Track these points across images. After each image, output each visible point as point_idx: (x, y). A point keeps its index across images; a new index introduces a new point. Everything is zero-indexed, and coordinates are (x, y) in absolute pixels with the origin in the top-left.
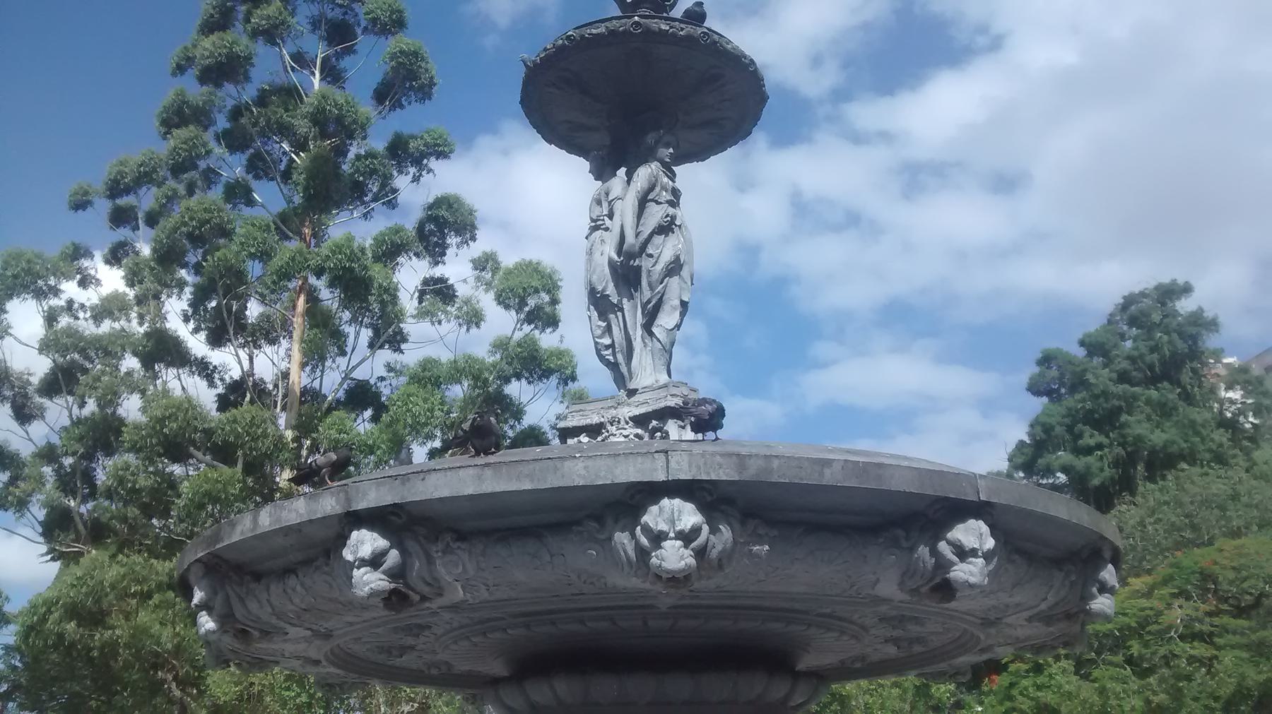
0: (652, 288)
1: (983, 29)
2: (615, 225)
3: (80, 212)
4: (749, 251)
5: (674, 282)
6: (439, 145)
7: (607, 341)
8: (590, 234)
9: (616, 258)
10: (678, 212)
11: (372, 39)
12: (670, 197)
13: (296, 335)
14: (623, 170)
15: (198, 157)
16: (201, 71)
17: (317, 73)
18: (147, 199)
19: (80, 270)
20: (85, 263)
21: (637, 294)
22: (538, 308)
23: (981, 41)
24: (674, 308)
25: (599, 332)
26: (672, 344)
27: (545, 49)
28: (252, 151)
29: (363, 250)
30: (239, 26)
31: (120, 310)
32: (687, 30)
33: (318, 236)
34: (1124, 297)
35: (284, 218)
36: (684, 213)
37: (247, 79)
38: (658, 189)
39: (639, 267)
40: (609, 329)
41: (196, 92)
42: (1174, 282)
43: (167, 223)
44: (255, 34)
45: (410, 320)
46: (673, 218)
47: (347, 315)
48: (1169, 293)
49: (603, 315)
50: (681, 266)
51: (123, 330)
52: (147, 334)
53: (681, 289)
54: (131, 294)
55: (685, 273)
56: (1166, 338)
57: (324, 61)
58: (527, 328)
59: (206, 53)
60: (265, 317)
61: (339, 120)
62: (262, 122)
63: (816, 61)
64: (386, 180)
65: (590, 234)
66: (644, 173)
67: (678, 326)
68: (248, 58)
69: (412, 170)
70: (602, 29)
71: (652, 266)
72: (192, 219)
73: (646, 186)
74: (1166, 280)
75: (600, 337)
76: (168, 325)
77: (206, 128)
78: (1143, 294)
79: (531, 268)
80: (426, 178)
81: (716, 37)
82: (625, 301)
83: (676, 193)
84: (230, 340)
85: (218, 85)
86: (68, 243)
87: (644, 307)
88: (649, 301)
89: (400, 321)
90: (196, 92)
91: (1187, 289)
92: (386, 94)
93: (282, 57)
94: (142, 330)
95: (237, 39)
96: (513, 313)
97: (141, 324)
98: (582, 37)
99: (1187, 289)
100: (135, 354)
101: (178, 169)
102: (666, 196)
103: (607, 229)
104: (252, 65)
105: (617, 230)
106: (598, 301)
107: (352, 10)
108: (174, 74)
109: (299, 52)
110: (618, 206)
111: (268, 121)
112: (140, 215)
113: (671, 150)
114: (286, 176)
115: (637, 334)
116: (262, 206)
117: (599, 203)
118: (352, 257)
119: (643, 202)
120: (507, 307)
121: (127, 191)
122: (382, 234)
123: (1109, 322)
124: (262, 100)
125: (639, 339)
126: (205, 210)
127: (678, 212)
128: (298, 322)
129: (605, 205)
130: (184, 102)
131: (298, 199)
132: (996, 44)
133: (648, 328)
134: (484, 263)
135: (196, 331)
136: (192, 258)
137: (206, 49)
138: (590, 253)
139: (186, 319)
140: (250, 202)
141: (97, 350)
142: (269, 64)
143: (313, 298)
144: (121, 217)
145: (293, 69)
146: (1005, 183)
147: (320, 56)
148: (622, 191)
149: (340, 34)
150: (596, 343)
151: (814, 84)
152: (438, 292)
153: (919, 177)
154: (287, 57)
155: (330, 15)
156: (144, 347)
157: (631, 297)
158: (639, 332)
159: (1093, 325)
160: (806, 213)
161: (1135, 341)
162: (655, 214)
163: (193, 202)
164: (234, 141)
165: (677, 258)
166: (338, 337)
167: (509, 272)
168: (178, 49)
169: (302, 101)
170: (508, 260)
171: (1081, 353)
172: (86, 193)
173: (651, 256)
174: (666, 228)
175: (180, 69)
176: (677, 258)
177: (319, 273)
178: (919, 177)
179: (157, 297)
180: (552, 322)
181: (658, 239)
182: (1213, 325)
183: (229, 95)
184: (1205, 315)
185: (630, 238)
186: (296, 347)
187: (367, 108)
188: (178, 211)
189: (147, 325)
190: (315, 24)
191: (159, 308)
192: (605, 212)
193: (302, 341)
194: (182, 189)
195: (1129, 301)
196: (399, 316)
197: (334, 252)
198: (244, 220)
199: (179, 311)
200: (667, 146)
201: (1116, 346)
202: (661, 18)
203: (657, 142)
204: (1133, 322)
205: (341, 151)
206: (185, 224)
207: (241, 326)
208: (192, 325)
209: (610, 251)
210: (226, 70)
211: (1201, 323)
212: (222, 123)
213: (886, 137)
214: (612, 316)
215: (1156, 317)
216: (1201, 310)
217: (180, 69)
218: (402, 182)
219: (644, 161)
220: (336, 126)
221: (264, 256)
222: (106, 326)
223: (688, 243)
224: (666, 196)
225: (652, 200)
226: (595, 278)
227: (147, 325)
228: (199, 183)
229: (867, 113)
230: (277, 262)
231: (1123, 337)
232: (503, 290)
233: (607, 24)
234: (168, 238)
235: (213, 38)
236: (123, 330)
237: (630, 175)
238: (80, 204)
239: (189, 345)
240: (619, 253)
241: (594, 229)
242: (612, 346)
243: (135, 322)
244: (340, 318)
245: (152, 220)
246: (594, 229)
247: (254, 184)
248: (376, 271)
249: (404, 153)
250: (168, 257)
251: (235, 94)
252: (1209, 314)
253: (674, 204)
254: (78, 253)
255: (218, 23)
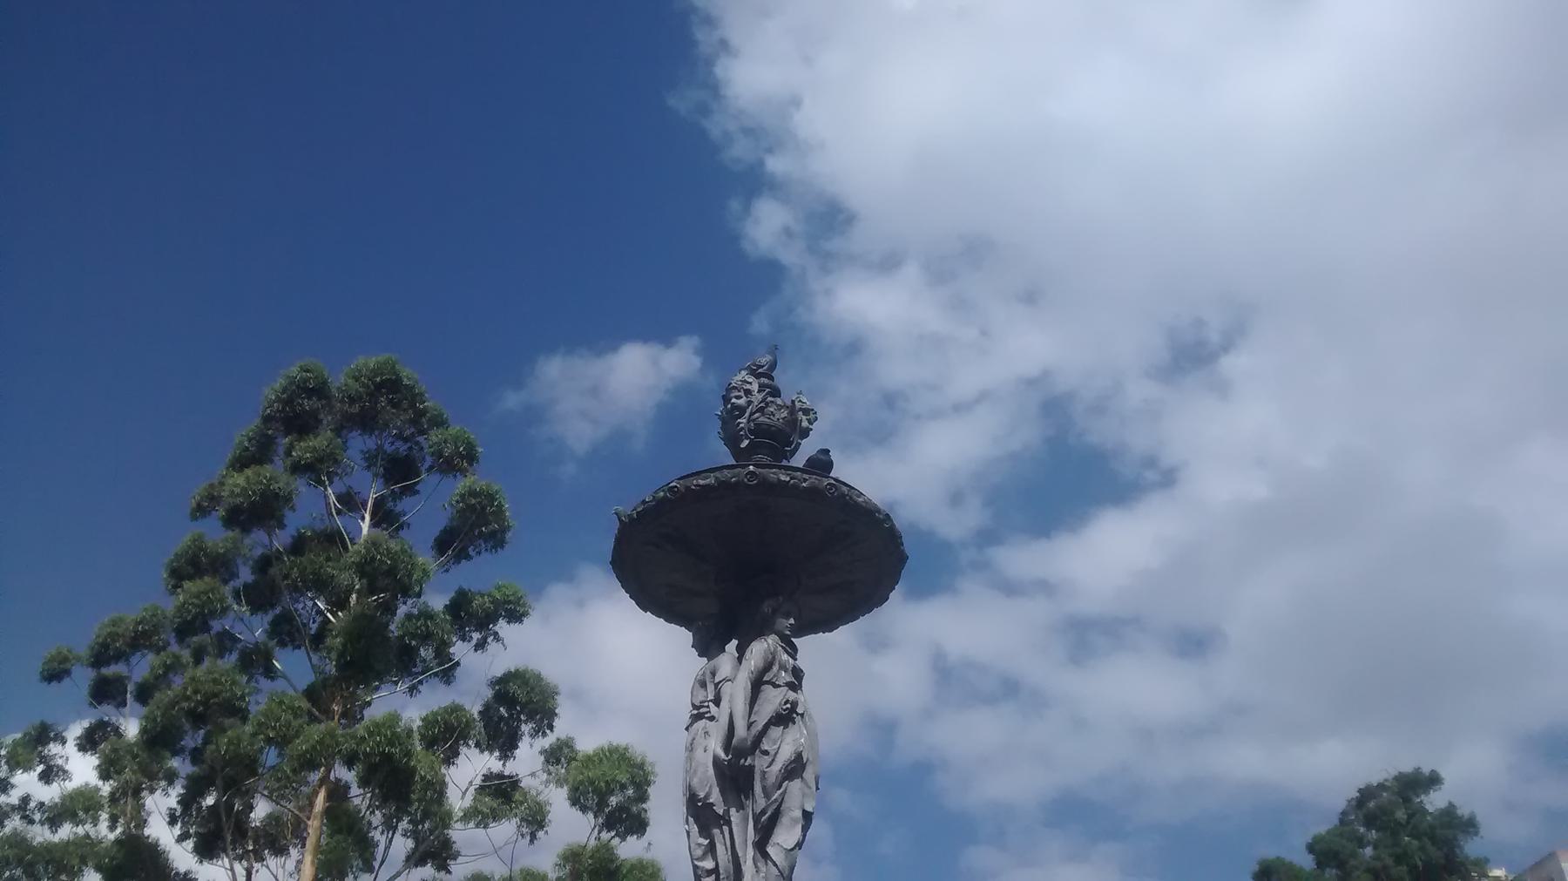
0: (767, 795)
1: (1151, 462)
2: (722, 713)
3: (54, 684)
4: (884, 729)
5: (795, 786)
6: (510, 602)
7: (709, 864)
8: (691, 725)
9: (723, 755)
10: (800, 697)
11: (434, 478)
12: (790, 678)
13: (310, 843)
14: (735, 642)
15: (213, 614)
16: (227, 511)
17: (367, 517)
18: (142, 667)
19: (44, 759)
20: (54, 748)
21: (749, 803)
22: (621, 808)
23: (1151, 475)
24: (795, 821)
25: (699, 852)
26: (792, 869)
27: (644, 502)
28: (278, 610)
29: (410, 732)
30: (278, 461)
31: (87, 811)
32: (809, 481)
33: (351, 716)
34: (1360, 790)
35: (311, 693)
36: (808, 697)
37: (282, 526)
38: (775, 668)
39: (752, 767)
40: (711, 849)
41: (216, 535)
42: (1417, 771)
43: (163, 697)
44: (297, 469)
45: (458, 825)
46: (795, 704)
47: (377, 818)
48: (1416, 783)
49: (705, 831)
50: (803, 767)
51: (87, 836)
52: (118, 842)
53: (804, 795)
54: (106, 788)
55: (809, 774)
56: (1415, 842)
57: (378, 503)
58: (605, 836)
59: (237, 490)
60: (272, 819)
61: (391, 572)
62: (295, 573)
63: (956, 499)
64: (442, 653)
65: (691, 725)
66: (758, 650)
67: (799, 845)
68: (288, 499)
69: (476, 636)
70: (711, 480)
71: (769, 767)
72: (196, 692)
73: (761, 664)
74: (1407, 767)
75: (701, 859)
76: (147, 832)
77: (226, 582)
78: (1381, 787)
79: (618, 756)
80: (492, 646)
81: (845, 489)
82: (733, 811)
83: (797, 673)
84: (225, 851)
85: (246, 530)
86: (37, 722)
87: (757, 819)
88: (763, 812)
89: (447, 826)
90: (216, 535)
91: (1434, 780)
92: (453, 544)
93: (326, 497)
94: (112, 837)
95: (275, 473)
96: (591, 815)
97: (112, 828)
98: (688, 488)
99: (1434, 780)
100: (98, 869)
101: (184, 631)
102: (785, 677)
103: (712, 718)
104: (293, 509)
105: (724, 720)
106: (701, 814)
107: (417, 443)
108: (194, 518)
109: (348, 494)
110: (726, 689)
111: (302, 572)
112: (129, 688)
113: (792, 621)
114: (318, 640)
115: (748, 855)
116: (285, 677)
117: (703, 685)
118: (394, 740)
119: (757, 685)
120: (584, 809)
121: (120, 656)
122: (435, 714)
123: (1342, 822)
124: (298, 546)
125: (750, 862)
126: (215, 681)
127: (800, 697)
128: (314, 825)
129: (711, 687)
130: (201, 549)
131: (331, 668)
132: (1169, 479)
133: (761, 846)
134: (557, 755)
135: (181, 839)
136: (191, 740)
137: (237, 485)
138: (691, 748)
139: (172, 821)
140: (270, 672)
141: (48, 863)
142: (311, 505)
143: (338, 793)
144: (106, 692)
145: (339, 512)
146: (1194, 644)
147: (373, 496)
148: (735, 668)
149: (400, 472)
150: (695, 867)
151: (955, 525)
152: (500, 793)
153: (1088, 636)
154: (333, 498)
155: (388, 448)
156: (112, 859)
157: (741, 807)
158: (750, 852)
159: (1322, 827)
160: (953, 681)
161: (1375, 848)
162: (773, 699)
163: (200, 672)
164: (259, 597)
165: (799, 756)
166: (365, 848)
167: (589, 760)
168: (205, 485)
169: (346, 549)
170: (587, 744)
171: (1307, 862)
172: (66, 660)
173: (766, 753)
174: (785, 717)
175: (200, 511)
176: (799, 756)
177: (350, 762)
178: (1088, 636)
179: (137, 793)
180: (637, 825)
181: (775, 732)
182: (1470, 826)
183: (257, 542)
184: (1459, 812)
185: (741, 731)
186: (308, 859)
187: (425, 558)
188: (178, 682)
189: (119, 830)
190: (370, 459)
191: (140, 807)
192: (711, 697)
193: (318, 849)
194: (186, 655)
195: (1366, 794)
196: (445, 820)
197: (371, 734)
198: (260, 698)
199: (164, 811)
200: (787, 618)
201: (1354, 855)
202: (780, 467)
203: (775, 611)
204: (1370, 821)
205: (389, 609)
206: (188, 699)
207: (241, 829)
208: (177, 830)
209: (715, 745)
210: (260, 511)
211: (1456, 824)
212: (246, 575)
213: (1044, 587)
214: (716, 831)
215: (1401, 815)
216: (1451, 805)
217: (200, 511)
218: (460, 650)
219: (760, 633)
220: (388, 578)
221: (282, 742)
222: (66, 831)
223: (812, 736)
224: (785, 677)
225: (768, 682)
226: (695, 782)
227: (119, 830)
228: (210, 649)
229: (1021, 559)
230: (301, 745)
231: (1361, 843)
232: (581, 782)
233: (718, 474)
234: (163, 715)
235: (248, 472)
236: (87, 836)
237: (741, 650)
238: (55, 673)
239: (171, 856)
240: (727, 746)
241: (696, 718)
242: (715, 871)
243: (103, 826)
244: (370, 823)
245: (144, 694)
246: (696, 718)
247: (277, 651)
248: (422, 759)
249: (476, 616)
250: (159, 740)
251: (266, 541)
252: (1464, 811)
253: (795, 686)
254: (43, 735)
255: (255, 454)
